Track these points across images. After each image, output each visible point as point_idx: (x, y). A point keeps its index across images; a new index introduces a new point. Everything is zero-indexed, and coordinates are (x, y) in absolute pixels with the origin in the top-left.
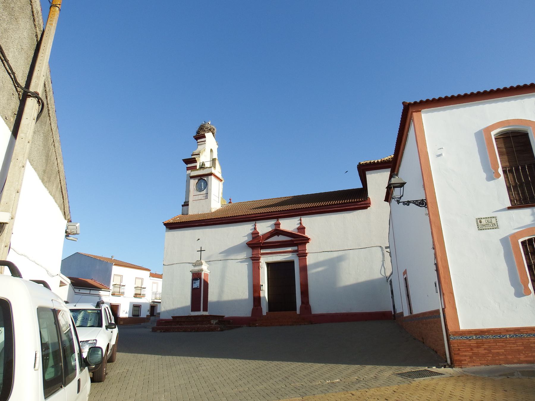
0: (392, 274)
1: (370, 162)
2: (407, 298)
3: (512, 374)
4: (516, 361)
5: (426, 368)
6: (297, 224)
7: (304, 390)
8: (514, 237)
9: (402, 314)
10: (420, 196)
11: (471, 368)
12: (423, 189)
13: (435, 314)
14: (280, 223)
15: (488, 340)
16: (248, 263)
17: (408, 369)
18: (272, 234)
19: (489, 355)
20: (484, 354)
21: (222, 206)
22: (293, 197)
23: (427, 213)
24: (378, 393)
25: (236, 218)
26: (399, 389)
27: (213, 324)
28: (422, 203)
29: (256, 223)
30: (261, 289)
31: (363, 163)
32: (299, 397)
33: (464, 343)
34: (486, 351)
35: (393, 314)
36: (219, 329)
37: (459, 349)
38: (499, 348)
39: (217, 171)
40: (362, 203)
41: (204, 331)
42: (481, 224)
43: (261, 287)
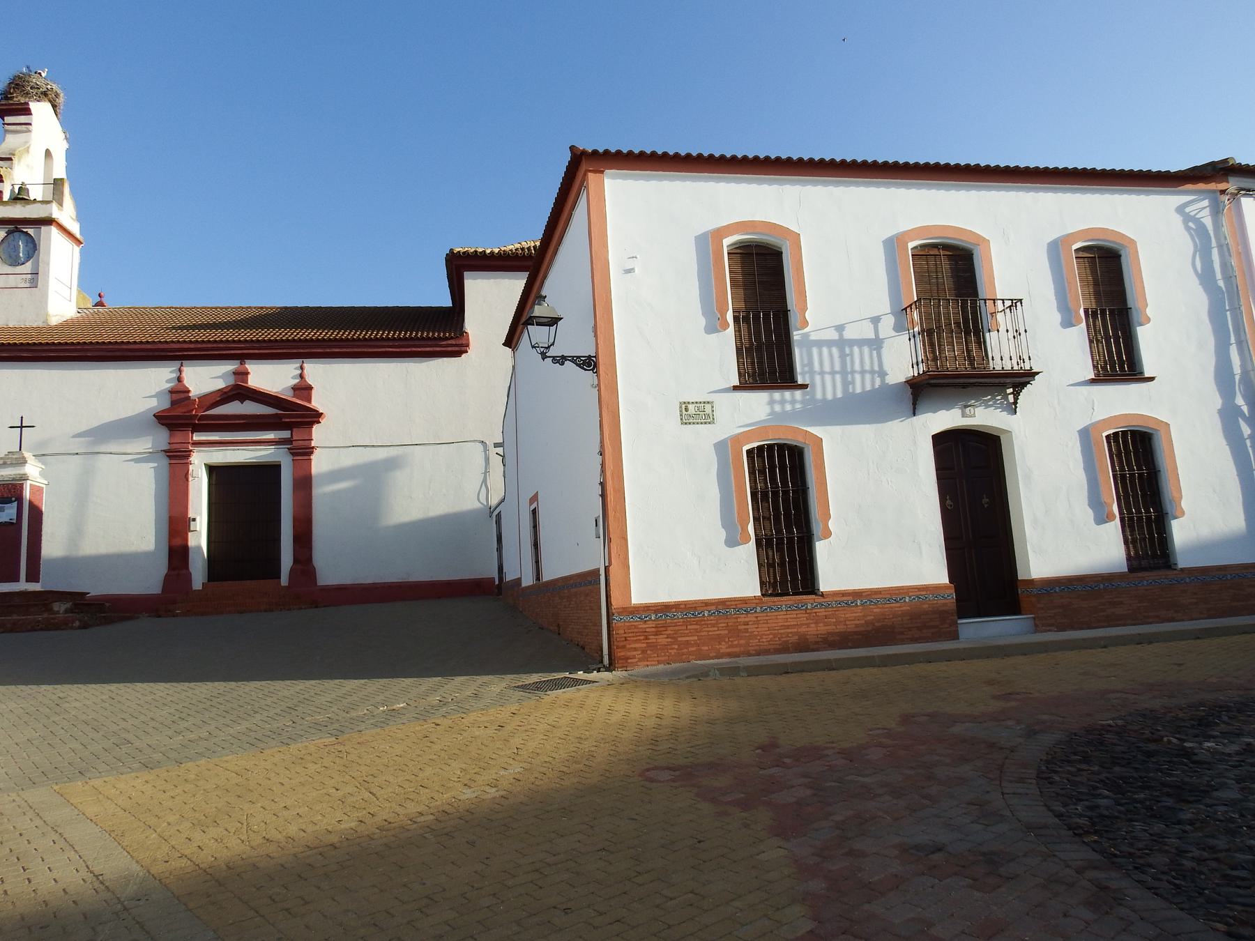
0: (503, 500)
1: (476, 251)
2: (533, 550)
3: (706, 674)
4: (714, 654)
5: (567, 674)
6: (292, 378)
7: (336, 726)
8: (737, 440)
9: (519, 581)
10: (586, 350)
11: (641, 669)
12: (593, 334)
13: (589, 579)
14: (249, 371)
15: (675, 621)
16: (156, 465)
17: (535, 678)
18: (225, 396)
19: (674, 646)
20: (665, 645)
21: (79, 310)
22: (281, 308)
23: (596, 382)
24: (484, 719)
25: (125, 347)
26: (521, 710)
27: (58, 612)
28: (588, 363)
29: (182, 365)
30: (192, 529)
31: (459, 252)
32: (328, 737)
33: (636, 627)
34: (669, 640)
35: (497, 583)
36: (77, 624)
37: (625, 638)
38: (690, 634)
39: (66, 214)
40: (449, 342)
41: (33, 630)
42: (687, 413)
43: (189, 523)
